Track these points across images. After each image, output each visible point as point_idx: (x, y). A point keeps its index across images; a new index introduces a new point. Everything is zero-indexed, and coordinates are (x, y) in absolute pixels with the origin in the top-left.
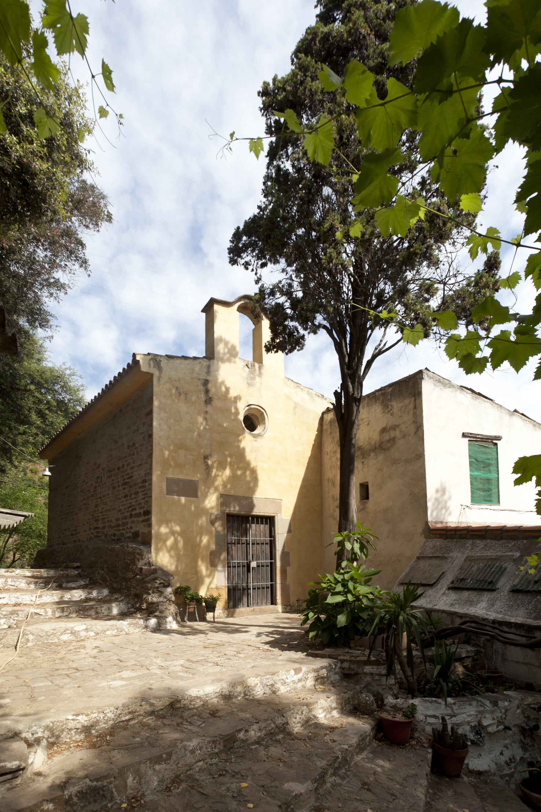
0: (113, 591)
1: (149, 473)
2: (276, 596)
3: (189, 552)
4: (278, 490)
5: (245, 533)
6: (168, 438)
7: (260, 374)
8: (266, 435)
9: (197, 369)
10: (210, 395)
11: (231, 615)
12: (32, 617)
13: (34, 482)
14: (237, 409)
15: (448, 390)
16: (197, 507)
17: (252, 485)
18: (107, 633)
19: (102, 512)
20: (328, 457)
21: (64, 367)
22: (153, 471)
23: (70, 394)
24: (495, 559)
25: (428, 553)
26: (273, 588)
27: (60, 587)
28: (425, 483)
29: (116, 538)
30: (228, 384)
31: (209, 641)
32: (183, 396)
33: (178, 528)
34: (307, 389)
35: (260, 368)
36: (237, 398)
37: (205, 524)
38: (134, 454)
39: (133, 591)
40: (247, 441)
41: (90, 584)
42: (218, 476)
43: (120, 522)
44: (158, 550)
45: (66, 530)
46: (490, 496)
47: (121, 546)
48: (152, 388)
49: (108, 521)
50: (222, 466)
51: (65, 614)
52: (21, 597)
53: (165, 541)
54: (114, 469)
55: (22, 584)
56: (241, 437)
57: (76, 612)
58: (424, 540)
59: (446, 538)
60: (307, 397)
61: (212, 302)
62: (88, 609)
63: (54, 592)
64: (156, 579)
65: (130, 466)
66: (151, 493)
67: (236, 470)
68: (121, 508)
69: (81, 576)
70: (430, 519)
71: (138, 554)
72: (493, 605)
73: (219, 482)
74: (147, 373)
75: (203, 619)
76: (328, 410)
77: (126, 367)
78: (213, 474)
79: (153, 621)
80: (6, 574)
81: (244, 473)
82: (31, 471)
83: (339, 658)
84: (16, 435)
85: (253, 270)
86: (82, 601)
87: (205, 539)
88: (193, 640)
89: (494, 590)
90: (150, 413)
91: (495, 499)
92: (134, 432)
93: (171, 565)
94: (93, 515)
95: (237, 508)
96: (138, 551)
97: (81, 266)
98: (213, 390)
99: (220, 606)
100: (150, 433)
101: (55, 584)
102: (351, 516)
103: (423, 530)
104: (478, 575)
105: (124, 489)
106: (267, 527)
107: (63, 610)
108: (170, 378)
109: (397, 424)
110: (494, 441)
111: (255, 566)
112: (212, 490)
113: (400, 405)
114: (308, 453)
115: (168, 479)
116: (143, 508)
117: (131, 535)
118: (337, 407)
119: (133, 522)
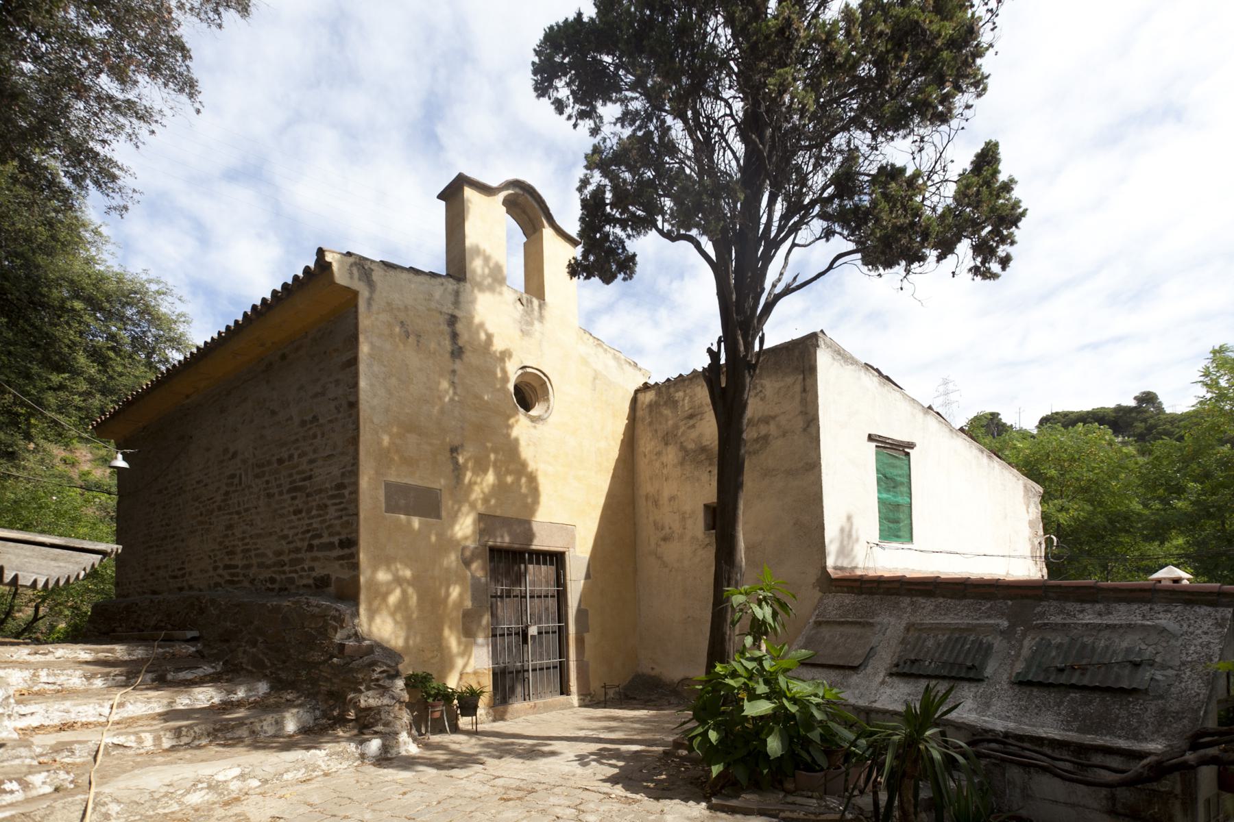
0: (278, 685)
1: (352, 471)
2: (568, 681)
3: (427, 613)
4: (570, 512)
5: (519, 579)
6: (387, 410)
7: (541, 318)
8: (550, 420)
9: (437, 294)
10: (460, 343)
11: (499, 717)
12: (107, 754)
13: (70, 479)
14: (504, 371)
15: (850, 367)
16: (440, 535)
17: (529, 500)
18: (285, 777)
19: (243, 539)
20: (646, 461)
21: (144, 277)
22: (361, 468)
23: (159, 327)
25: (833, 614)
26: (563, 669)
27: (161, 682)
29: (276, 586)
30: (490, 328)
31: (500, 782)
33: (408, 573)
35: (541, 307)
36: (505, 355)
37: (454, 565)
38: (315, 436)
39: (325, 687)
40: (521, 427)
41: (227, 672)
42: (475, 483)
43: (285, 558)
44: (372, 615)
45: (158, 568)
46: (899, 530)
47: (294, 603)
48: (356, 318)
49: (256, 555)
50: (481, 468)
51: (184, 740)
52: (74, 710)
53: (384, 596)
54: (269, 463)
55: (75, 680)
56: (512, 421)
57: (208, 735)
60: (612, 363)
61: (461, 182)
62: (233, 728)
63: (151, 694)
64: (373, 664)
65: (305, 460)
66: (357, 507)
67: (506, 475)
68: (286, 532)
69: (203, 657)
71: (334, 618)
72: (988, 705)
73: (476, 494)
74: (347, 289)
75: (455, 729)
77: (301, 274)
78: (467, 480)
79: (375, 745)
80: (33, 658)
81: (518, 480)
82: (64, 461)
83: (782, 815)
84: (42, 391)
85: (570, 117)
86: (212, 709)
87: (455, 592)
88: (467, 780)
89: (980, 680)
90: (353, 362)
91: (903, 533)
92: (316, 395)
93: (397, 637)
94: (220, 543)
95: (507, 539)
96: (333, 613)
97: (181, 90)
98: (464, 338)
99: (483, 702)
100: (352, 399)
101: (149, 676)
104: (942, 653)
105: (293, 498)
106: (554, 568)
107: (178, 733)
108: (389, 304)
109: (772, 414)
112: (465, 509)
113: (777, 385)
114: (614, 453)
115: (388, 486)
116: (339, 534)
117: (311, 582)
118: (711, 374)
119: (314, 559)
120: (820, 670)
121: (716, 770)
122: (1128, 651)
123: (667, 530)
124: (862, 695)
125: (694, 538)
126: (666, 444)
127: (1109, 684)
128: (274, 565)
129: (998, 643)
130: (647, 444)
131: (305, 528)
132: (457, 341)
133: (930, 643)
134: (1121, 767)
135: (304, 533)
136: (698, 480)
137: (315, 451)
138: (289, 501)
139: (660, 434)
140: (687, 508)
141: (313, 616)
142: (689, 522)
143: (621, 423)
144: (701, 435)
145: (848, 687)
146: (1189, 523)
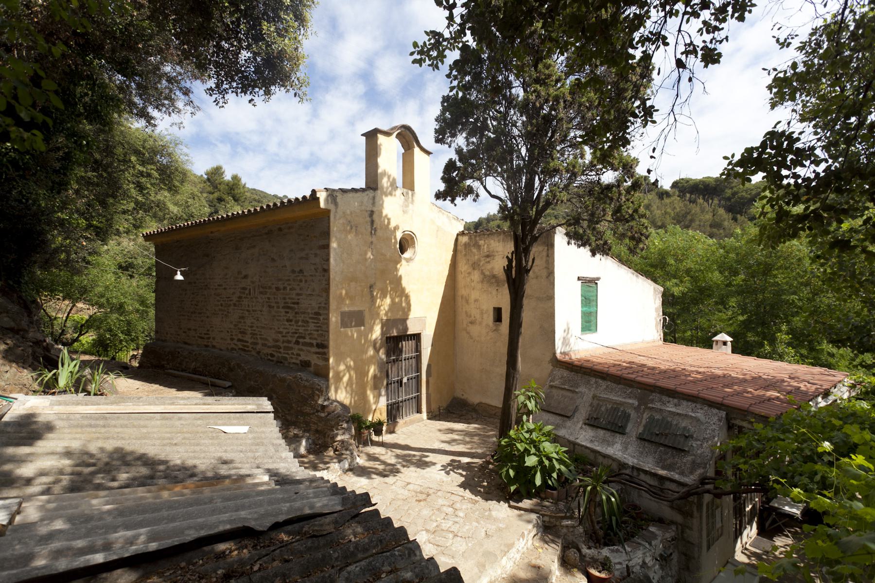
1: (325, 307)
19: (252, 327)
21: (166, 133)
26: (418, 399)
31: (411, 487)
32: (354, 228)
35: (412, 195)
36: (396, 228)
38: (301, 281)
39: (314, 427)
43: (280, 344)
46: (590, 326)
54: (270, 288)
56: (398, 266)
58: (551, 367)
59: (572, 371)
65: (294, 292)
68: (281, 330)
70: (558, 352)
71: (318, 390)
72: (626, 448)
76: (462, 234)
89: (624, 434)
91: (593, 328)
92: (301, 258)
94: (235, 325)
100: (325, 267)
105: (287, 312)
114: (446, 273)
119: (301, 350)
121: (513, 488)
122: (685, 428)
124: (571, 434)
125: (487, 325)
127: (675, 446)
128: (273, 347)
129: (633, 414)
130: (463, 267)
132: (373, 220)
133: (603, 409)
134: (677, 490)
137: (301, 289)
138: (284, 313)
140: (484, 307)
141: (305, 387)
142: (485, 316)
143: (450, 253)
144: (493, 268)
145: (565, 427)
146: (741, 292)
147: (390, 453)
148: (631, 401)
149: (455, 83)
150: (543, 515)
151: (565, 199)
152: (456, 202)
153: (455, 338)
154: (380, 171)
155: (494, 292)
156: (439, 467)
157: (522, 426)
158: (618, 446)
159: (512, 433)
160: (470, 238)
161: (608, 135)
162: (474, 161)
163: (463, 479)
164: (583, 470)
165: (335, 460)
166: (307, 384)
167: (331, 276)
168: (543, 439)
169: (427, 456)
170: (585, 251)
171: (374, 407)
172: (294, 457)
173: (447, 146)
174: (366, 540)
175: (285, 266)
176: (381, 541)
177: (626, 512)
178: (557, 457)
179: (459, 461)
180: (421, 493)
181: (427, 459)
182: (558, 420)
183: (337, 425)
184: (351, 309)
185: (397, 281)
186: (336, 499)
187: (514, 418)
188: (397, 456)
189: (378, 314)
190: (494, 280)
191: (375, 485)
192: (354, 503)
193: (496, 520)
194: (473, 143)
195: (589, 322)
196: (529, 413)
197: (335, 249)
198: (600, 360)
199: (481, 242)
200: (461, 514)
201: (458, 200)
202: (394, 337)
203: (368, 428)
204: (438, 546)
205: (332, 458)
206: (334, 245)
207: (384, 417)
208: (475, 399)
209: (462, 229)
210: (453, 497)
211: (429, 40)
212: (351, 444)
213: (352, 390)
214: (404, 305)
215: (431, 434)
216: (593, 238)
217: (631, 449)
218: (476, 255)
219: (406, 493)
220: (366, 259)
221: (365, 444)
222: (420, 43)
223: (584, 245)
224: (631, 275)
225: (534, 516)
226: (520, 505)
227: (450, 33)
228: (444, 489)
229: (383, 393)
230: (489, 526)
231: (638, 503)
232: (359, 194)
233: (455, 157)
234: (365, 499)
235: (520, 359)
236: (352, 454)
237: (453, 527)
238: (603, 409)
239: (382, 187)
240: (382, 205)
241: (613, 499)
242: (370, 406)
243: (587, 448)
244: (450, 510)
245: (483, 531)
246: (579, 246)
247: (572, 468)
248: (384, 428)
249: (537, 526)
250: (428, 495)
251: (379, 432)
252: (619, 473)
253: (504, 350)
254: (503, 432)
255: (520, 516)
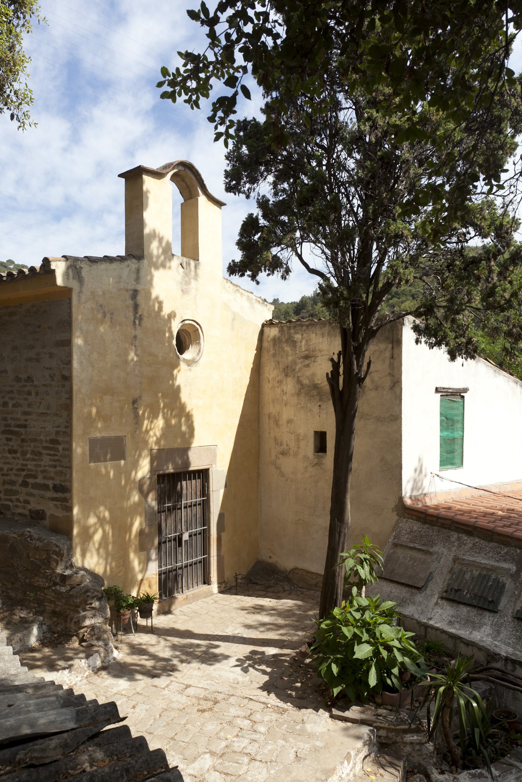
1: (66, 431)
2: (209, 573)
20: (270, 385)
24: (490, 570)
25: (404, 539)
26: (205, 564)
28: (401, 451)
31: (191, 691)
34: (247, 294)
35: (196, 267)
36: (172, 316)
38: (29, 393)
39: (49, 607)
46: (454, 458)
47: (20, 536)
48: (70, 308)
50: (154, 416)
56: (175, 372)
58: (397, 518)
59: (425, 523)
60: (246, 304)
71: (55, 553)
72: (499, 632)
76: (269, 324)
78: (144, 429)
83: (375, 724)
89: (497, 612)
91: (457, 461)
92: (30, 359)
98: (142, 305)
100: (65, 373)
102: (346, 517)
103: (396, 506)
110: (462, 394)
111: (187, 538)
114: (246, 381)
117: (27, 512)
119: (31, 495)
120: (396, 585)
121: (336, 691)
123: (285, 446)
124: (423, 612)
125: (306, 457)
126: (286, 375)
129: (509, 584)
130: (271, 372)
131: (19, 466)
132: (137, 304)
133: (468, 576)
135: (18, 470)
136: (311, 410)
137: (29, 405)
139: (281, 366)
140: (301, 431)
141: (37, 548)
142: (302, 444)
143: (252, 353)
144: (313, 375)
145: (414, 603)
147: (163, 643)
148: (506, 565)
149: (222, 129)
150: (378, 728)
151: (411, 278)
152: (258, 278)
153: (258, 476)
154: (147, 231)
155: (316, 409)
156: (233, 661)
157: (351, 603)
158: (487, 629)
159: (336, 611)
160: (281, 331)
161: (444, 201)
162: (285, 218)
163: (266, 678)
164: (436, 663)
165: (82, 655)
166: (39, 544)
167: (75, 388)
168: (380, 620)
169: (217, 647)
170: (441, 353)
171: (140, 577)
172: (14, 654)
173: (243, 196)
174: (107, 770)
175: (5, 371)
176: (127, 770)
177: (494, 721)
178: (399, 646)
179: (263, 653)
180: (206, 699)
181: (217, 651)
182: (404, 592)
183: (84, 604)
184: (105, 434)
185: (174, 393)
186: (68, 713)
187: (340, 591)
188: (174, 647)
189: (146, 442)
190: (315, 392)
191: (138, 690)
192: (93, 718)
193: (311, 736)
194: (284, 190)
195: (452, 452)
196: (361, 583)
197: (79, 347)
198: (465, 507)
199: (298, 337)
200: (262, 729)
201: (262, 276)
202: (169, 475)
203: (131, 607)
204: (227, 774)
205: (77, 652)
206: (78, 341)
207: (154, 591)
208: (287, 563)
209: (269, 317)
210: (253, 705)
211: (185, 65)
212: (105, 632)
213: (107, 553)
214: (184, 428)
215: (223, 615)
216: (452, 335)
217: (504, 633)
218: (290, 355)
219: (184, 699)
220: (126, 362)
221: (127, 630)
222: (172, 70)
223: (438, 344)
224: (512, 384)
225: (365, 730)
226: (347, 714)
227: (216, 54)
228: (238, 693)
229: (154, 556)
230: (301, 745)
231: (512, 708)
232: (115, 265)
233: (257, 212)
234: (111, 711)
235: (349, 506)
236: (106, 645)
237: (250, 747)
238: (468, 576)
239: (151, 255)
240: (150, 282)
241: (475, 705)
242: (134, 576)
243: (443, 632)
244: (246, 723)
245: (292, 751)
246: (431, 346)
247: (421, 660)
248: (155, 607)
249: (369, 743)
250: (216, 702)
251: (146, 613)
252: (486, 668)
253: (328, 493)
254: (325, 612)
255: (346, 729)
